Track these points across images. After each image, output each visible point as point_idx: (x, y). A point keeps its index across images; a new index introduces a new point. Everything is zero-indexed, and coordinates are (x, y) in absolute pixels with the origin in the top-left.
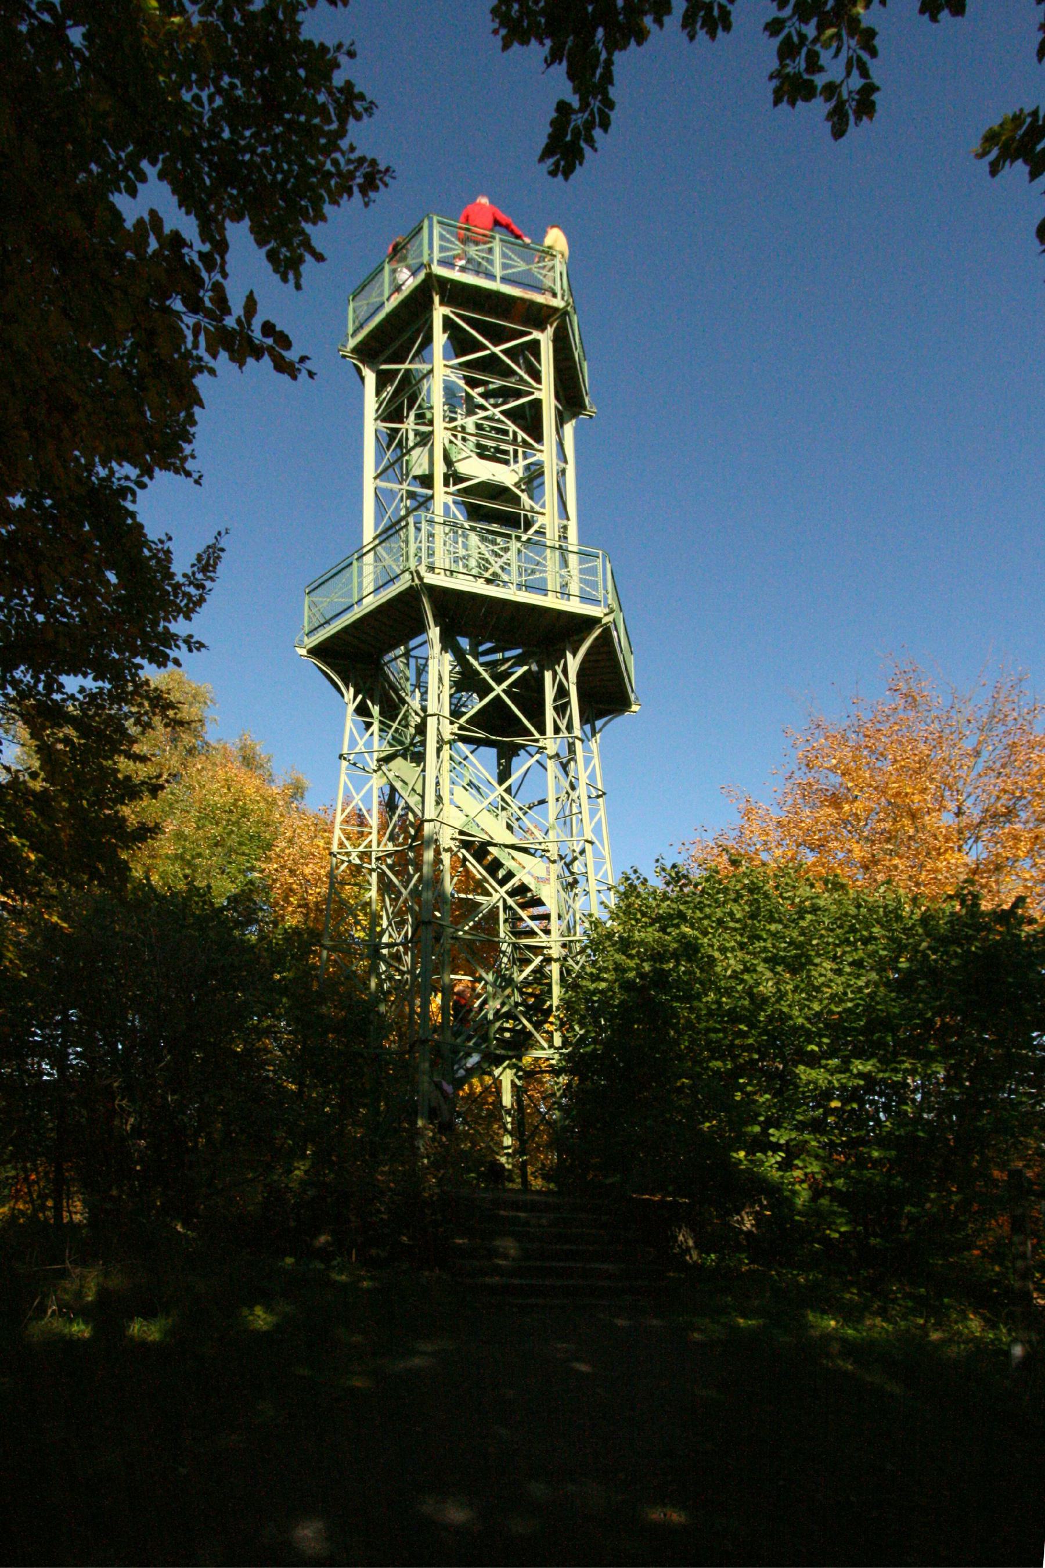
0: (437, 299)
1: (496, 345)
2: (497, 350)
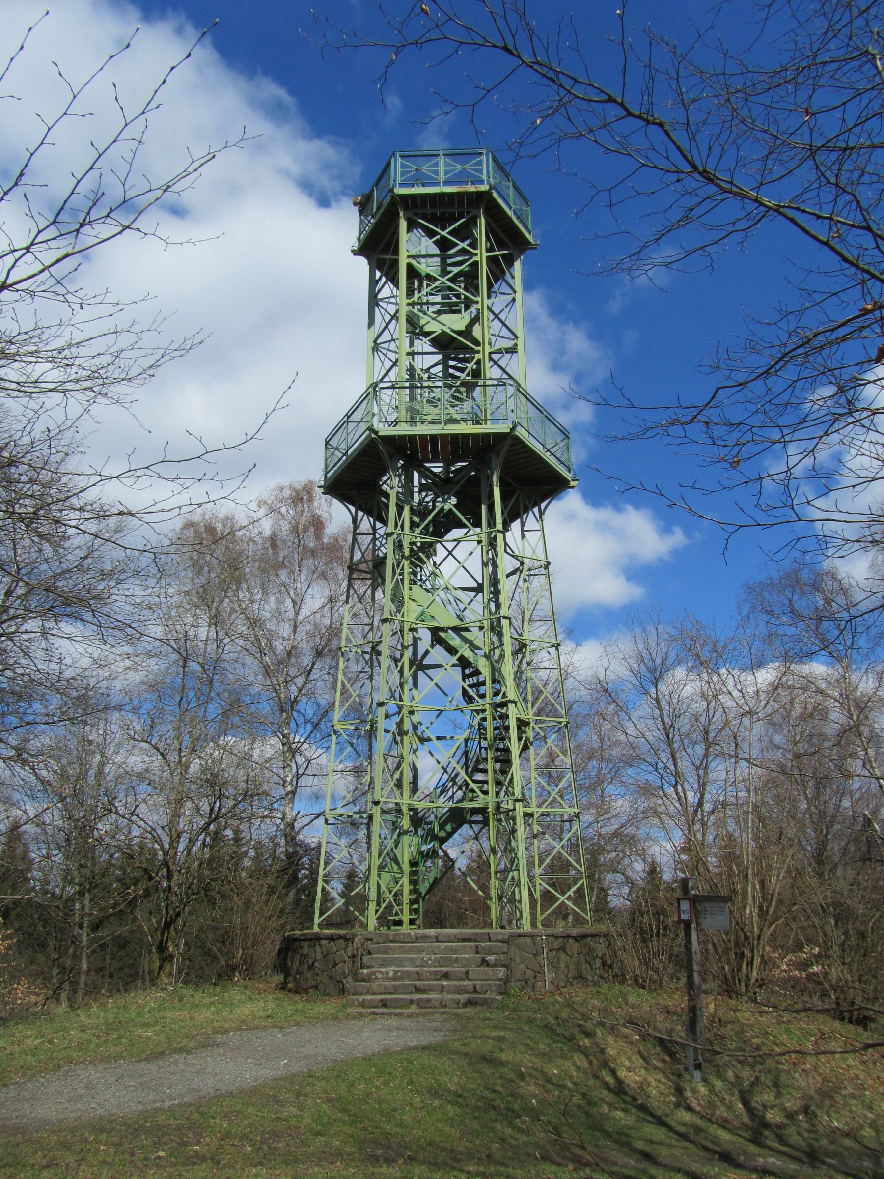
0: (403, 224)
1: (443, 229)
2: (444, 233)
